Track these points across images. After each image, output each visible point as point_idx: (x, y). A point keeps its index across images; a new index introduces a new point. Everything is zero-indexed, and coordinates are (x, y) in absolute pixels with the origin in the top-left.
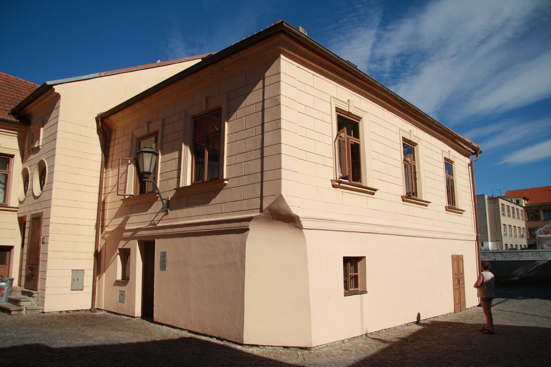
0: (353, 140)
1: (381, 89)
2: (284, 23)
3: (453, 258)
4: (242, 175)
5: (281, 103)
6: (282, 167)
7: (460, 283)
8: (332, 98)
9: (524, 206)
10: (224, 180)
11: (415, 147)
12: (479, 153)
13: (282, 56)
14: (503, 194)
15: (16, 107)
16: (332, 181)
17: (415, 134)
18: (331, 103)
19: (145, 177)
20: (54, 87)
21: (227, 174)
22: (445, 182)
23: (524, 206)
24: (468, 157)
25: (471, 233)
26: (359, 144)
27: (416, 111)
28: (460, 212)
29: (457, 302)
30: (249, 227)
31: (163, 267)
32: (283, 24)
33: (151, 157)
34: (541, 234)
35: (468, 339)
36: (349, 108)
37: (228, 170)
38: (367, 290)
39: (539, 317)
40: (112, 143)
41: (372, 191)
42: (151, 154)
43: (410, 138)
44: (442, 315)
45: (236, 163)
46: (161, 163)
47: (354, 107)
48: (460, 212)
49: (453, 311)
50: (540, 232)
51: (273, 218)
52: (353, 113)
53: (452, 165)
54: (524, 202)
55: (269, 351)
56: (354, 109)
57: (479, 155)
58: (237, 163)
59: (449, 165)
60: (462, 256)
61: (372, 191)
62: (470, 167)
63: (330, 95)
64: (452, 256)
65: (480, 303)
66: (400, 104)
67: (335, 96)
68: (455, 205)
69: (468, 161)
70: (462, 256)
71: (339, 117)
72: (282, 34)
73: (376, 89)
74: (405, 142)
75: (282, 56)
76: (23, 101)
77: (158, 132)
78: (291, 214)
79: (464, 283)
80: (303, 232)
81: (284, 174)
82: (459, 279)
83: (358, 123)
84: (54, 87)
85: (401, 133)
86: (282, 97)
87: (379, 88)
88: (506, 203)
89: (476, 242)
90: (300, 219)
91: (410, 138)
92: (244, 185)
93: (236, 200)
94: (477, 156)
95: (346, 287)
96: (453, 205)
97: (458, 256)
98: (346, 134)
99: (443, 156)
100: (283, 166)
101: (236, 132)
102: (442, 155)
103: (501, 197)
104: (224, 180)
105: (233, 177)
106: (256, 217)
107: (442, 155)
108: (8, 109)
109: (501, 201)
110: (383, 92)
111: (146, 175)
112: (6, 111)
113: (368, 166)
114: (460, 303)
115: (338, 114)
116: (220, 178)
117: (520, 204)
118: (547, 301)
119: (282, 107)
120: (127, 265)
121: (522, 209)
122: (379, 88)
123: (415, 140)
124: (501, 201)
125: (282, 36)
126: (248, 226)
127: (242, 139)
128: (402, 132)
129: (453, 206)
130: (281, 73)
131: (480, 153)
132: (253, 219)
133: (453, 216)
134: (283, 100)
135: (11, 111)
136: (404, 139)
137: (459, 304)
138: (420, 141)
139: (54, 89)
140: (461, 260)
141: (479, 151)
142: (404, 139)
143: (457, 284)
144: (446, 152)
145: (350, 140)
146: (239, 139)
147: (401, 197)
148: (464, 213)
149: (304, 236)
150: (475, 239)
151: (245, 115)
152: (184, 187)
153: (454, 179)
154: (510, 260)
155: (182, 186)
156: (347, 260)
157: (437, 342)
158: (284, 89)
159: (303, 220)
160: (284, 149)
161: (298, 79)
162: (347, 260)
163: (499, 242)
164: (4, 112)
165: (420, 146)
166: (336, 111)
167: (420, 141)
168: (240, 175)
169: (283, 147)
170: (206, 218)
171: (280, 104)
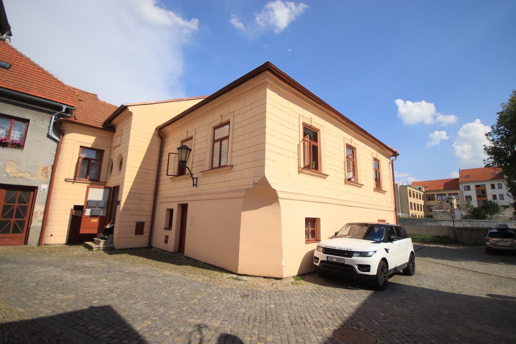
9: (424, 191)
14: (410, 184)
15: (106, 120)
18: (299, 119)
20: (128, 107)
23: (424, 191)
24: (389, 159)
25: (391, 206)
28: (384, 192)
32: (268, 64)
34: (436, 209)
40: (166, 144)
41: (325, 176)
46: (344, 259)
48: (384, 192)
50: (435, 208)
54: (424, 189)
55: (198, 331)
56: (315, 123)
57: (397, 156)
59: (376, 160)
61: (325, 176)
67: (303, 115)
71: (305, 129)
76: (110, 117)
77: (192, 138)
81: (267, 162)
83: (317, 133)
84: (128, 107)
88: (412, 189)
90: (277, 192)
94: (396, 157)
98: (309, 139)
102: (372, 155)
103: (409, 186)
107: (372, 155)
108: (102, 122)
109: (408, 188)
112: (101, 123)
117: (421, 190)
118: (514, 267)
120: (83, 212)
121: (423, 193)
124: (408, 188)
125: (268, 73)
133: (379, 195)
135: (104, 123)
139: (128, 109)
145: (312, 143)
148: (386, 193)
149: (280, 205)
150: (394, 210)
153: (380, 171)
156: (308, 220)
160: (267, 147)
162: (308, 220)
163: (407, 213)
164: (99, 123)
166: (303, 124)
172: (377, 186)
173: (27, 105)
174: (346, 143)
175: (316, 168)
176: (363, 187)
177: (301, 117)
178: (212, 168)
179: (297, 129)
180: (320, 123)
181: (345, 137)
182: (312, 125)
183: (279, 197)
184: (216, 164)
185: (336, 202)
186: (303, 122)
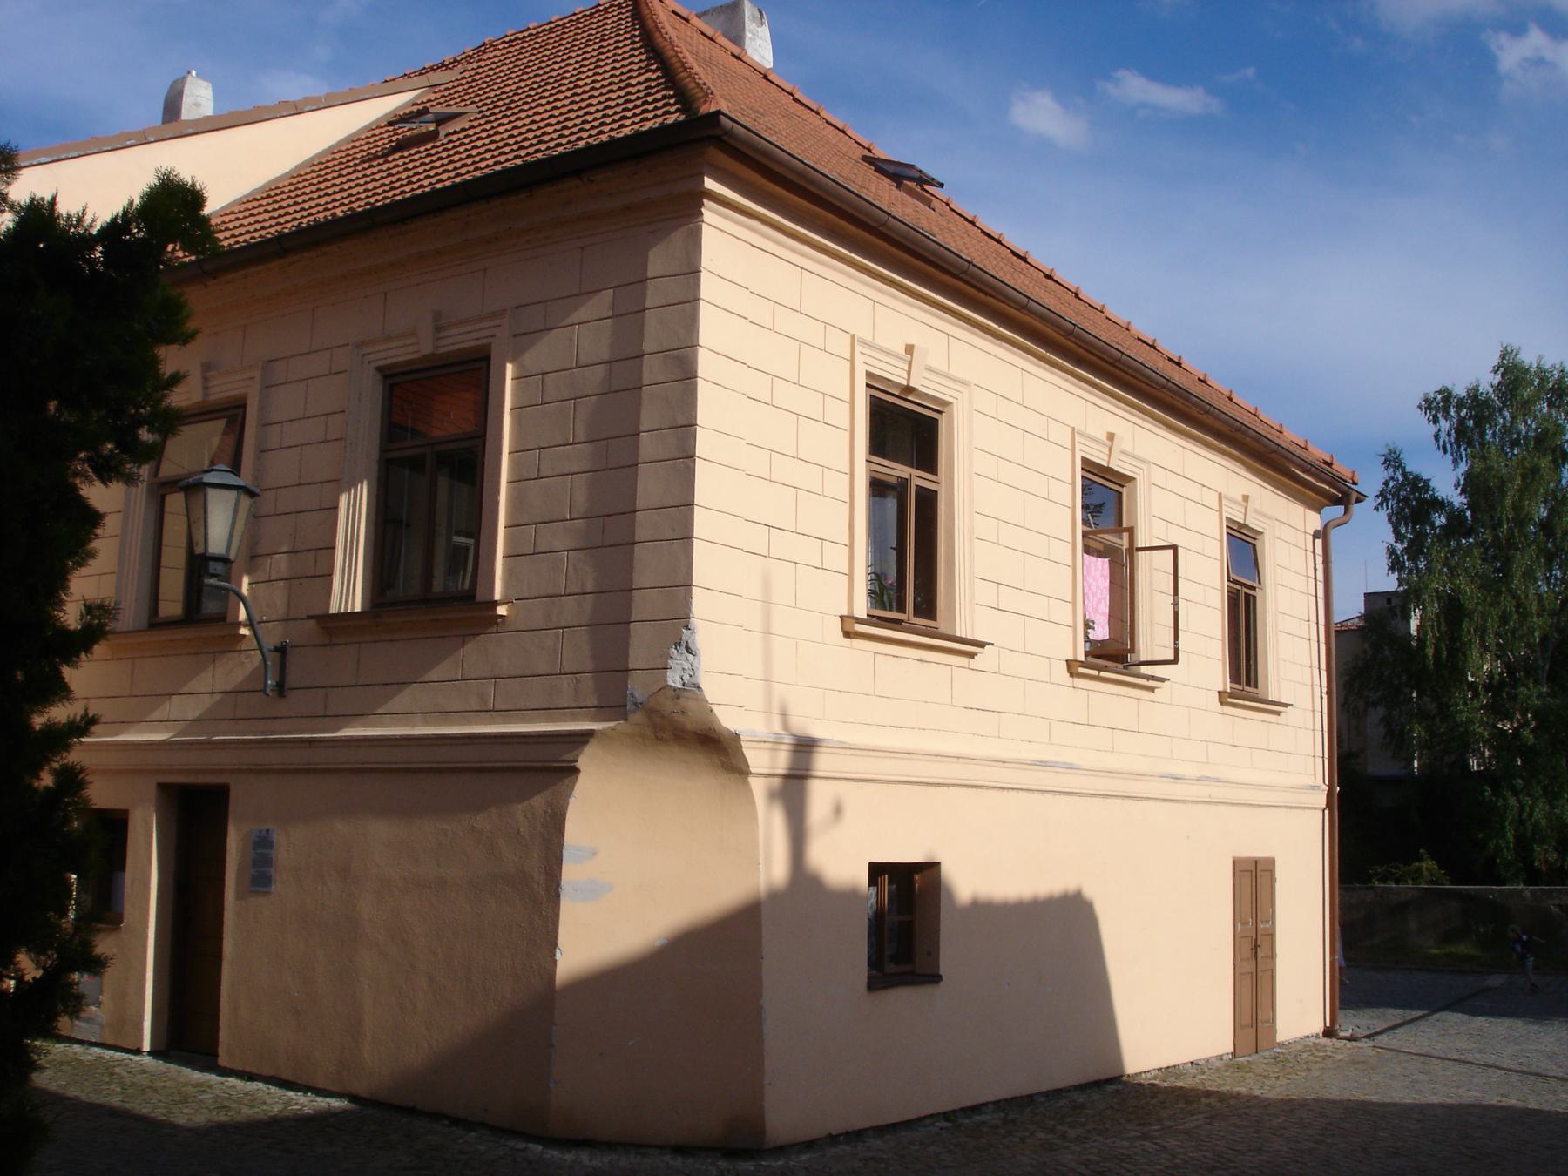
0: (916, 478)
1: (1018, 307)
2: (722, 117)
3: (1237, 870)
4: (558, 592)
5: (699, 375)
6: (694, 583)
7: (1260, 954)
8: (856, 342)
10: (496, 604)
11: (1124, 491)
12: (1354, 499)
13: (705, 201)
16: (845, 619)
17: (1128, 448)
19: (212, 571)
21: (507, 584)
22: (1223, 608)
24: (1318, 511)
26: (937, 420)
27: (1135, 370)
28: (1276, 707)
29: (1246, 1020)
30: (578, 765)
31: (260, 877)
32: (718, 121)
33: (231, 505)
35: (1255, 1135)
36: (909, 373)
37: (509, 573)
38: (942, 972)
39: (1503, 1072)
42: (233, 495)
43: (1108, 462)
44: (1192, 1063)
45: (537, 551)
47: (926, 369)
48: (1276, 707)
49: (1231, 1049)
51: (657, 738)
52: (921, 389)
53: (1254, 545)
56: (927, 374)
58: (542, 549)
60: (1271, 861)
62: (1319, 542)
63: (852, 333)
64: (1234, 862)
65: (1328, 1025)
66: (1081, 350)
67: (868, 337)
68: (1256, 687)
69: (1314, 521)
70: (1271, 861)
72: (711, 148)
73: (1003, 305)
74: (1092, 473)
75: (705, 201)
78: (716, 728)
79: (1272, 956)
80: (746, 783)
82: (1256, 940)
85: (1078, 446)
86: (700, 350)
87: (1012, 304)
89: (1327, 812)
91: (1108, 462)
92: (564, 625)
93: (535, 673)
95: (875, 962)
96: (1248, 684)
97: (1256, 862)
99: (1221, 515)
100: (698, 576)
101: (538, 449)
102: (1220, 512)
104: (496, 604)
105: (527, 596)
106: (603, 733)
107: (1220, 512)
110: (1026, 314)
111: (215, 567)
113: (960, 426)
114: (1255, 1023)
115: (871, 396)
116: (480, 597)
119: (703, 389)
122: (1012, 304)
123: (1126, 466)
126: (577, 761)
127: (559, 472)
128: (1083, 441)
129: (1247, 688)
130: (702, 274)
131: (1358, 501)
132: (592, 740)
133: (1246, 723)
134: (705, 364)
136: (1088, 465)
137: (1252, 1026)
138: (1142, 469)
140: (1269, 873)
141: (1354, 496)
142: (1088, 465)
143: (1248, 959)
144: (1236, 502)
146: (550, 474)
147: (1065, 663)
151: (573, 396)
152: (347, 614)
154: (172, 1065)
155: (340, 607)
157: (1156, 1144)
158: (713, 329)
159: (751, 748)
161: (748, 292)
165: (1141, 486)
167: (1142, 469)
168: (550, 592)
169: (700, 516)
170: (427, 723)
171: (696, 377)
172: (1235, 677)
173: (1100, 671)
174: (1084, 460)
175: (927, 606)
176: (985, 657)
177: (858, 348)
178: (155, 623)
179: (839, 413)
180: (1138, 452)
181: (1079, 427)
182: (1247, 523)
183: (752, 770)
184: (172, 605)
185: (1100, 785)
186: (869, 375)
